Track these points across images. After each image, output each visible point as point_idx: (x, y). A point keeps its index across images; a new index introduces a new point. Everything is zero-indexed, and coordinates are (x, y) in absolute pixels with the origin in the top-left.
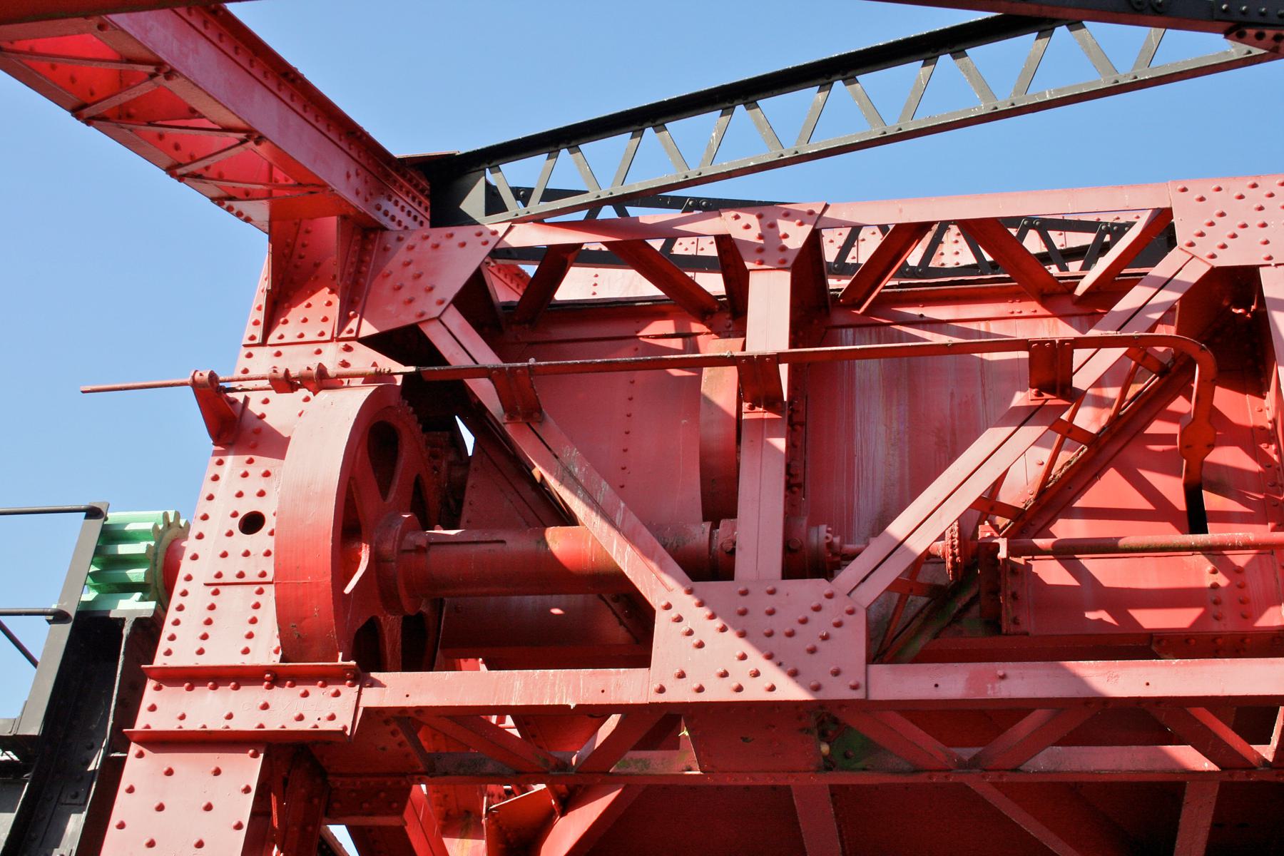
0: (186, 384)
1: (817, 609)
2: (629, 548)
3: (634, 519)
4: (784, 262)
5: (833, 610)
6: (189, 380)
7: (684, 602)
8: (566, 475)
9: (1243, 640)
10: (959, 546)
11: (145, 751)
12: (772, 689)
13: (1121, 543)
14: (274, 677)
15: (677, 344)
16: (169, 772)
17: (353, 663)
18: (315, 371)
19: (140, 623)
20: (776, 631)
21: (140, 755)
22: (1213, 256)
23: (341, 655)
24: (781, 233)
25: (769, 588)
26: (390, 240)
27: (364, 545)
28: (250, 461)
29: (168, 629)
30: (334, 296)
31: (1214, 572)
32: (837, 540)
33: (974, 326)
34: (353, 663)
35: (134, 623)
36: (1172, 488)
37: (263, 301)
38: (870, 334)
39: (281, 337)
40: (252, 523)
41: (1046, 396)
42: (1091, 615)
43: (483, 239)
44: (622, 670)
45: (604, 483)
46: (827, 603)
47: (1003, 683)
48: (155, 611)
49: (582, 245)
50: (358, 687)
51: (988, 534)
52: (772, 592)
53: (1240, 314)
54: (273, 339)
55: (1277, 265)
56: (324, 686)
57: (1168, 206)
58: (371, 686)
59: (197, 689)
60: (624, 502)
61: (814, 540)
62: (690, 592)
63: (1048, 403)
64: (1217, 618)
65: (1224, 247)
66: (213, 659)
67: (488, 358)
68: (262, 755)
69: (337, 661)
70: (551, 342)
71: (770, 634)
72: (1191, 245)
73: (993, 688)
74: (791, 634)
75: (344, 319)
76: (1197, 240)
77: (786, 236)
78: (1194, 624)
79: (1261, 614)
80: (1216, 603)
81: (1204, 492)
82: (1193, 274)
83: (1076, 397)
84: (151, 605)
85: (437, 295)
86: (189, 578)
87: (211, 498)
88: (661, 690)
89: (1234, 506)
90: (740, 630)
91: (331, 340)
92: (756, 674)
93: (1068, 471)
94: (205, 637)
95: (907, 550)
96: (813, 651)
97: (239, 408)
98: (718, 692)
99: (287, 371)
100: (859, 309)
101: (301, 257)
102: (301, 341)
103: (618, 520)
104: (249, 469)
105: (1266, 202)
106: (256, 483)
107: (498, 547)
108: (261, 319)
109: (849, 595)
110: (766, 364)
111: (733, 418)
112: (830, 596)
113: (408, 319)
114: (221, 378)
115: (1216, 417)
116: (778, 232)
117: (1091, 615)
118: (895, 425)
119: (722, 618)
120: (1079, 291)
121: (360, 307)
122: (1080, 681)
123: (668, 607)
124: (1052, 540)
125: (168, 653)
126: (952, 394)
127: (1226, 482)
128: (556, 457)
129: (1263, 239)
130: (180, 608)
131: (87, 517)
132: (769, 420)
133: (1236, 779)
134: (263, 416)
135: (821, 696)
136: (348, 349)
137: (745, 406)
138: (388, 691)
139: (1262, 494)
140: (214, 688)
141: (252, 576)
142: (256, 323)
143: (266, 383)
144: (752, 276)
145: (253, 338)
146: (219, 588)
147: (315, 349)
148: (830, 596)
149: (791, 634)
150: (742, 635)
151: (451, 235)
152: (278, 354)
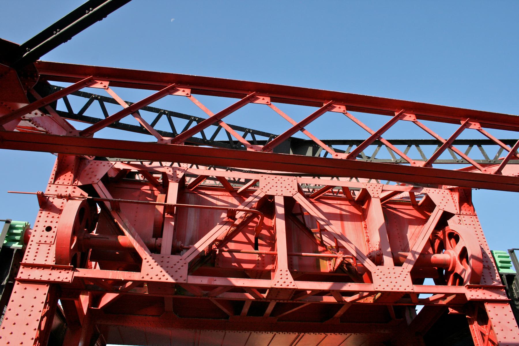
0: (35, 194)
1: (178, 262)
2: (138, 244)
3: (139, 237)
4: (177, 181)
5: (182, 263)
6: (36, 193)
7: (149, 258)
8: (125, 225)
9: (262, 271)
10: (208, 251)
11: (19, 283)
12: (167, 279)
13: (241, 251)
14: (53, 268)
15: (150, 192)
16: (26, 289)
17: (72, 266)
18: (68, 195)
19: (18, 250)
20: (169, 266)
21: (18, 284)
22: (266, 192)
23: (70, 264)
24: (177, 174)
25: (168, 256)
26: (87, 162)
27: (75, 237)
28: (49, 213)
29: (26, 253)
30: (72, 174)
31: (259, 257)
32: (183, 245)
33: (215, 196)
34: (72, 266)
35: (17, 250)
36: (252, 238)
37: (54, 173)
38: (193, 195)
39: (58, 183)
40: (49, 229)
41: (230, 219)
42: (233, 264)
43: (109, 165)
44: (134, 272)
45: (133, 228)
46: (180, 261)
47: (215, 282)
48: (22, 247)
49: (131, 170)
50: (73, 271)
51: (215, 247)
52: (169, 258)
53: (270, 201)
54: (56, 183)
55: (278, 196)
56: (65, 270)
57: (258, 179)
58: (76, 271)
59: (33, 269)
60: (138, 233)
61: (178, 244)
62: (151, 256)
63: (230, 221)
64: (258, 267)
65: (268, 190)
66: (37, 262)
67: (110, 197)
68: (49, 286)
69: (68, 265)
70: (122, 188)
71: (167, 267)
72: (262, 189)
73: (213, 282)
74: (172, 267)
75: (74, 181)
76: (263, 188)
77: (178, 175)
78: (254, 267)
79: (266, 266)
80: (258, 263)
81: (258, 239)
82: (262, 195)
83: (236, 219)
84: (21, 246)
85: (97, 177)
86: (32, 241)
87: (38, 221)
88: (143, 278)
89: (264, 243)
90: (161, 265)
91: (70, 185)
92: (164, 276)
93: (232, 232)
94: (36, 256)
95: (198, 251)
96: (176, 271)
97: (47, 200)
98: (155, 279)
99: (61, 194)
100: (191, 189)
101: (64, 163)
102: (63, 184)
103: (136, 237)
104: (49, 215)
105: (278, 181)
106: (50, 219)
107: (107, 239)
108: (54, 177)
109: (185, 259)
110: (171, 207)
111: (161, 214)
112: (181, 260)
113: (90, 182)
114: (44, 194)
115: (264, 224)
116: (176, 173)
117: (233, 264)
118: (196, 217)
119: (157, 262)
120: (239, 191)
121: (78, 178)
122: (230, 282)
123: (146, 259)
124: (228, 249)
125: (26, 259)
126: (209, 212)
127: (263, 238)
128: (123, 221)
129: (276, 190)
130: (30, 248)
131: (6, 223)
132: (171, 218)
133: (258, 301)
134: (53, 202)
135: (178, 281)
136: (75, 188)
137: (166, 214)
138: (80, 273)
139: (269, 241)
140: (38, 269)
141: (48, 242)
142: (52, 178)
143: (56, 196)
144: (170, 183)
145: (51, 182)
146: (40, 244)
147: (67, 187)
148: (181, 260)
149: (172, 267)
150: (161, 267)
151: (101, 163)
152: (57, 187)
